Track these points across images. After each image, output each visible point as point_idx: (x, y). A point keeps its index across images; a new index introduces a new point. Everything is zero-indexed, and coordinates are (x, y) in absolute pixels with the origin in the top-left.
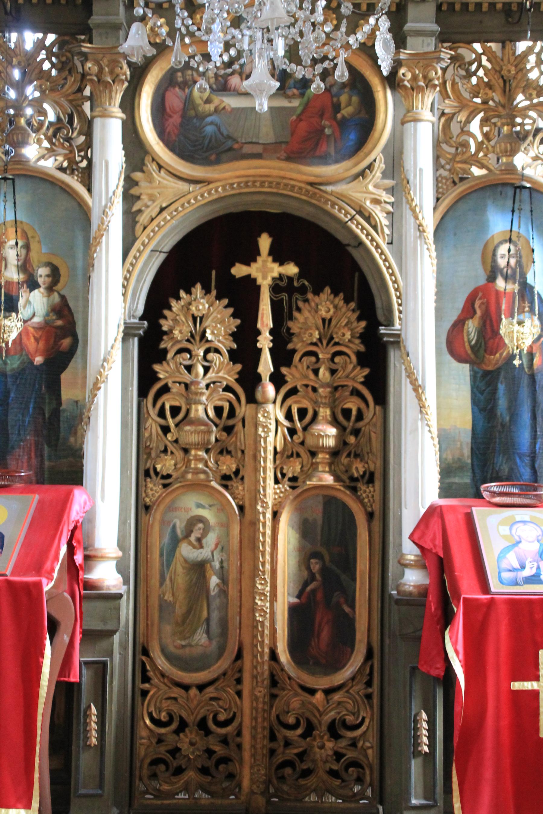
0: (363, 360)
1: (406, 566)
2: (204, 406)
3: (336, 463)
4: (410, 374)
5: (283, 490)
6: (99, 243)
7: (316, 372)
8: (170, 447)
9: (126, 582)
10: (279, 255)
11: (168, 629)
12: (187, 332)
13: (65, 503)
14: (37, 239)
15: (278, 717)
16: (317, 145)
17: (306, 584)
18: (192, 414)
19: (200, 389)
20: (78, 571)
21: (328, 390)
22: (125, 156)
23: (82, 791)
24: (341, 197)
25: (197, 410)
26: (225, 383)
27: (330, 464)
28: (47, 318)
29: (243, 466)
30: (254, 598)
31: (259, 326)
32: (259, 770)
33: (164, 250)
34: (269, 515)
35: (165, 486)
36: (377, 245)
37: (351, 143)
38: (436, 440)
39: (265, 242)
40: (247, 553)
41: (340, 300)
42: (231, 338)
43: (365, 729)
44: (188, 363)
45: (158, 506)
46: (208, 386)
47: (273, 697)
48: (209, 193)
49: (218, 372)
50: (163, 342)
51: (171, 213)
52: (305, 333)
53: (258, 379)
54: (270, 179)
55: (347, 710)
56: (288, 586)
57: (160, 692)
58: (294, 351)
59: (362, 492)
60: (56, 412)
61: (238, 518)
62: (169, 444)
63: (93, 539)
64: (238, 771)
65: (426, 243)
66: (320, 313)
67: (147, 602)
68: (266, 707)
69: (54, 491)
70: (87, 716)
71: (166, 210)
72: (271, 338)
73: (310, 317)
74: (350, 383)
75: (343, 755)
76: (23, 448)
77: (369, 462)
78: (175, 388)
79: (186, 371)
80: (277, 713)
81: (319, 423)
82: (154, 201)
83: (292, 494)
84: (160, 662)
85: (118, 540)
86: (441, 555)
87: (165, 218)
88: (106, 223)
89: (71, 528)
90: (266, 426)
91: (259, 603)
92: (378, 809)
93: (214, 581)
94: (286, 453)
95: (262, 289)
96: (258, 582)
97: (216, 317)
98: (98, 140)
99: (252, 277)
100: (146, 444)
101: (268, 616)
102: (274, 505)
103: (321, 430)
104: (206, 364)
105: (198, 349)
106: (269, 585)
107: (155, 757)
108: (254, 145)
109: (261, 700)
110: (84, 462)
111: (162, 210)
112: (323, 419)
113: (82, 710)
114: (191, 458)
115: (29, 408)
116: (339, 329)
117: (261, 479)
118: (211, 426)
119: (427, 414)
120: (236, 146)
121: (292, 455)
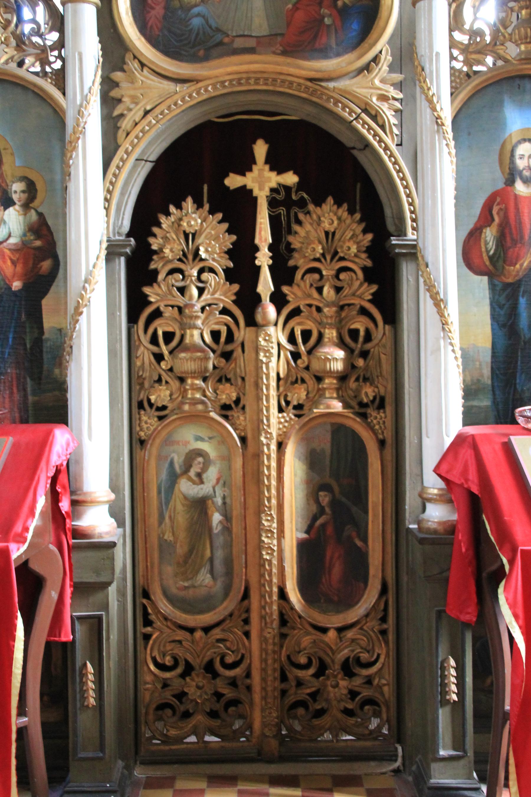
0: (370, 276)
1: (430, 500)
2: (200, 331)
3: (343, 389)
4: (431, 288)
5: (288, 419)
6: (75, 148)
7: (320, 290)
8: (165, 377)
9: (121, 524)
10: (276, 164)
11: (169, 570)
12: (179, 250)
13: (44, 444)
14: (10, 151)
15: (289, 657)
16: (315, 37)
17: (315, 519)
18: (187, 340)
19: (195, 312)
20: (64, 519)
21: (334, 309)
22: (102, 49)
23: (82, 755)
24: (345, 94)
25: (192, 336)
26: (222, 306)
27: (338, 390)
28: (24, 238)
29: (244, 394)
30: (260, 536)
31: (257, 241)
32: (270, 713)
33: (150, 159)
34: (274, 447)
35: (160, 418)
36: (387, 147)
37: (354, 34)
38: (460, 360)
39: (260, 149)
40: (252, 488)
41: (344, 211)
42: (227, 256)
43: (380, 666)
44: (180, 284)
45: (154, 439)
46: (203, 309)
47: (283, 636)
48: (198, 93)
49: (213, 294)
50: (153, 263)
51: (157, 116)
52: (307, 248)
53: (258, 299)
54: (265, 75)
55: (362, 648)
56: (296, 521)
57: (164, 635)
58: (295, 268)
59: (372, 418)
60: (38, 341)
61: (241, 450)
62: (163, 373)
63: (81, 482)
64: (249, 713)
65: (445, 138)
66: (323, 225)
67: (146, 543)
68: (276, 649)
69: (32, 432)
70: (83, 675)
71: (151, 113)
72: (271, 254)
73: (312, 230)
74: (356, 301)
75: (358, 693)
76: (4, 383)
77: (379, 385)
78: (168, 312)
79: (179, 294)
80: (288, 653)
81: (324, 345)
82: (137, 104)
83: (297, 423)
84: (162, 606)
85: (111, 480)
86: (475, 490)
87: (150, 122)
88: (82, 125)
89: (51, 473)
90: (269, 350)
91: (266, 540)
92: (396, 749)
93: (217, 518)
94: (290, 379)
95: (259, 201)
96: (264, 518)
97: (210, 233)
98: (70, 29)
99: (248, 187)
100: (138, 374)
101: (275, 554)
102: (279, 435)
103: (328, 353)
104: (201, 285)
105: (191, 269)
106: (275, 521)
107: (160, 702)
108: (247, 39)
109: (271, 641)
110: (69, 396)
111: (147, 113)
112: (330, 341)
113: (77, 668)
114: (188, 387)
115: (8, 338)
116: (344, 242)
117: (264, 408)
118: (208, 352)
119: (450, 332)
120: (226, 40)
121: (296, 382)
